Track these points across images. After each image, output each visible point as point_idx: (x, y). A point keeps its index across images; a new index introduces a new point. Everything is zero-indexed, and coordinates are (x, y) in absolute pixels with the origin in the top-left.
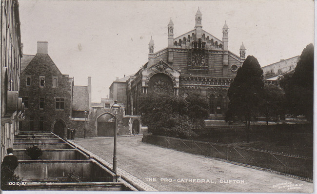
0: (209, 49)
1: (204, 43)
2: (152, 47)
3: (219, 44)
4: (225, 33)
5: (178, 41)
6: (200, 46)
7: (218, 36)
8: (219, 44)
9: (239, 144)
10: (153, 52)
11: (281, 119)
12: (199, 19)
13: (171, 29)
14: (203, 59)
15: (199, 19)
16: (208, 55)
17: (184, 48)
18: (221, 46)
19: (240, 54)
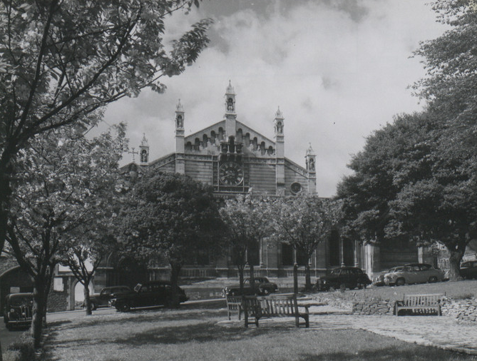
0: (250, 156)
1: (240, 146)
2: (312, 160)
3: (267, 145)
4: (280, 125)
5: (193, 142)
6: (232, 150)
7: (269, 133)
8: (267, 145)
9: (203, 310)
10: (146, 161)
11: (380, 265)
12: (230, 101)
13: (180, 118)
14: (240, 172)
15: (230, 101)
16: (248, 165)
17: (206, 154)
18: (271, 150)
19: (307, 164)
